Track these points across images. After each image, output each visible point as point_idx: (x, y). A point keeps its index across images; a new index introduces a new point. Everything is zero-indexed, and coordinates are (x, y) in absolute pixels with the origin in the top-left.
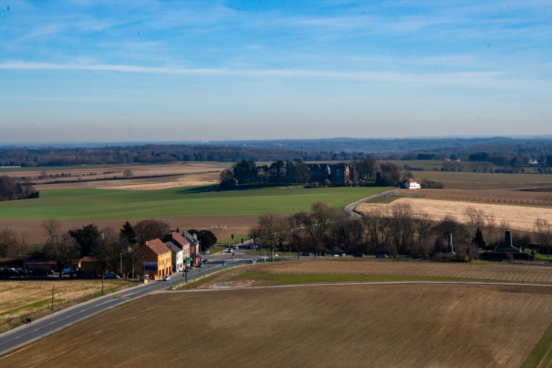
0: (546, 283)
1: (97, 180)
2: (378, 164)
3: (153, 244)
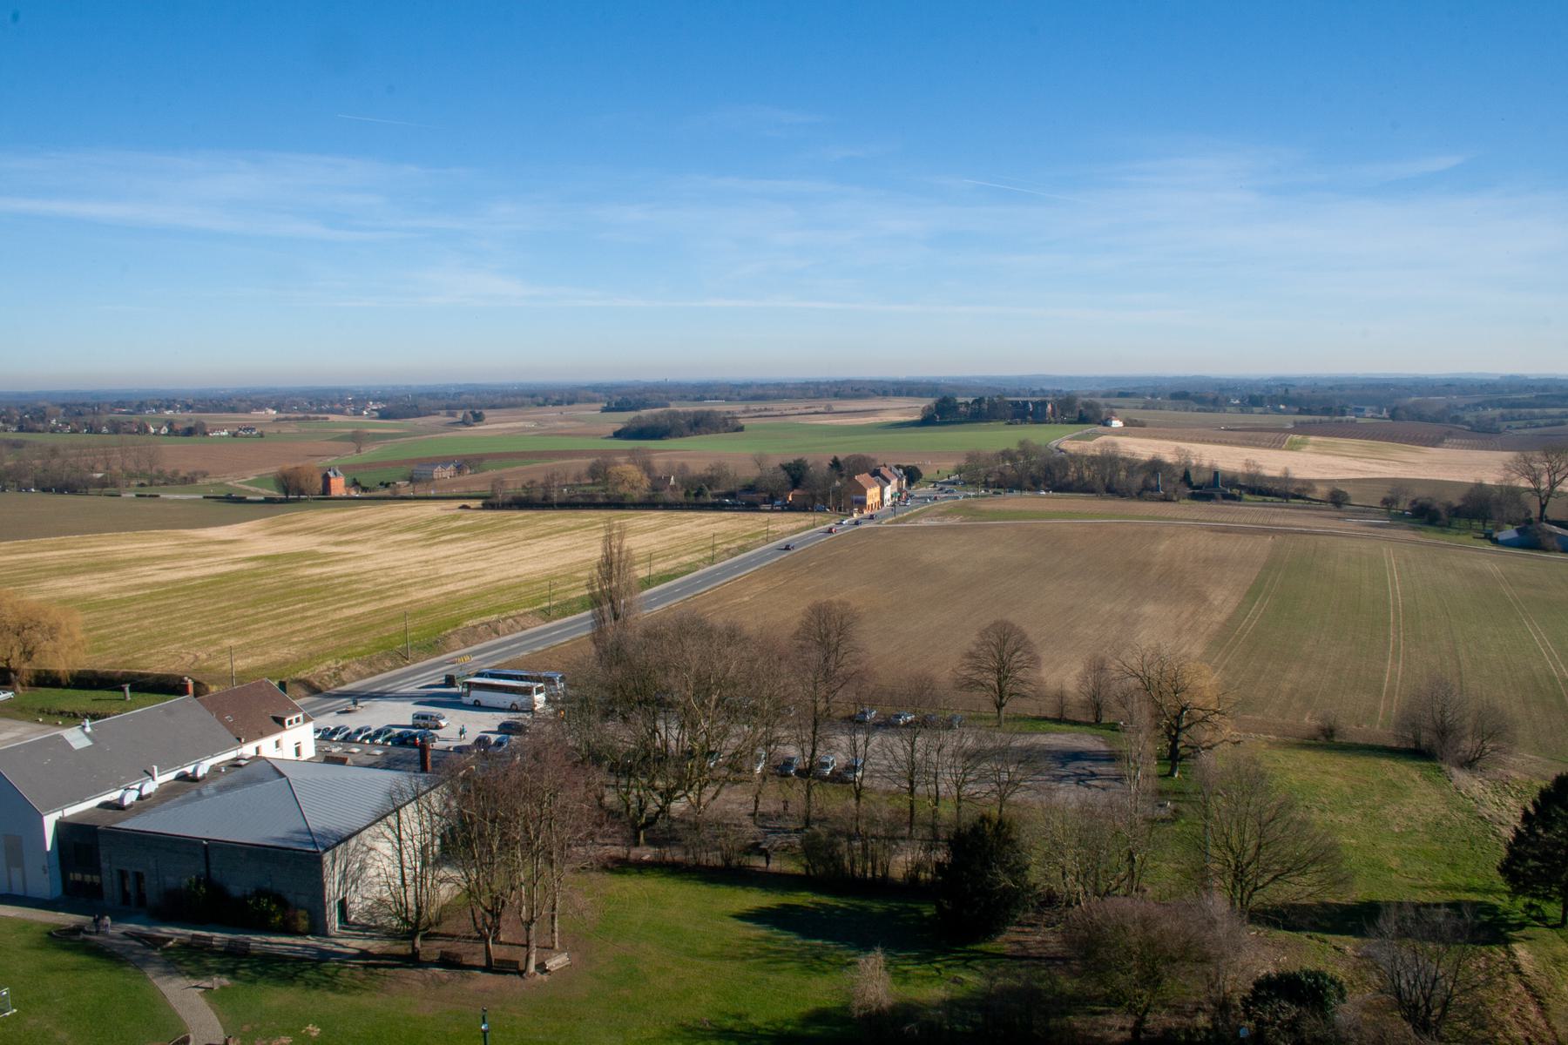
0: (1226, 522)
1: (799, 414)
2: (1078, 403)
3: (863, 478)
